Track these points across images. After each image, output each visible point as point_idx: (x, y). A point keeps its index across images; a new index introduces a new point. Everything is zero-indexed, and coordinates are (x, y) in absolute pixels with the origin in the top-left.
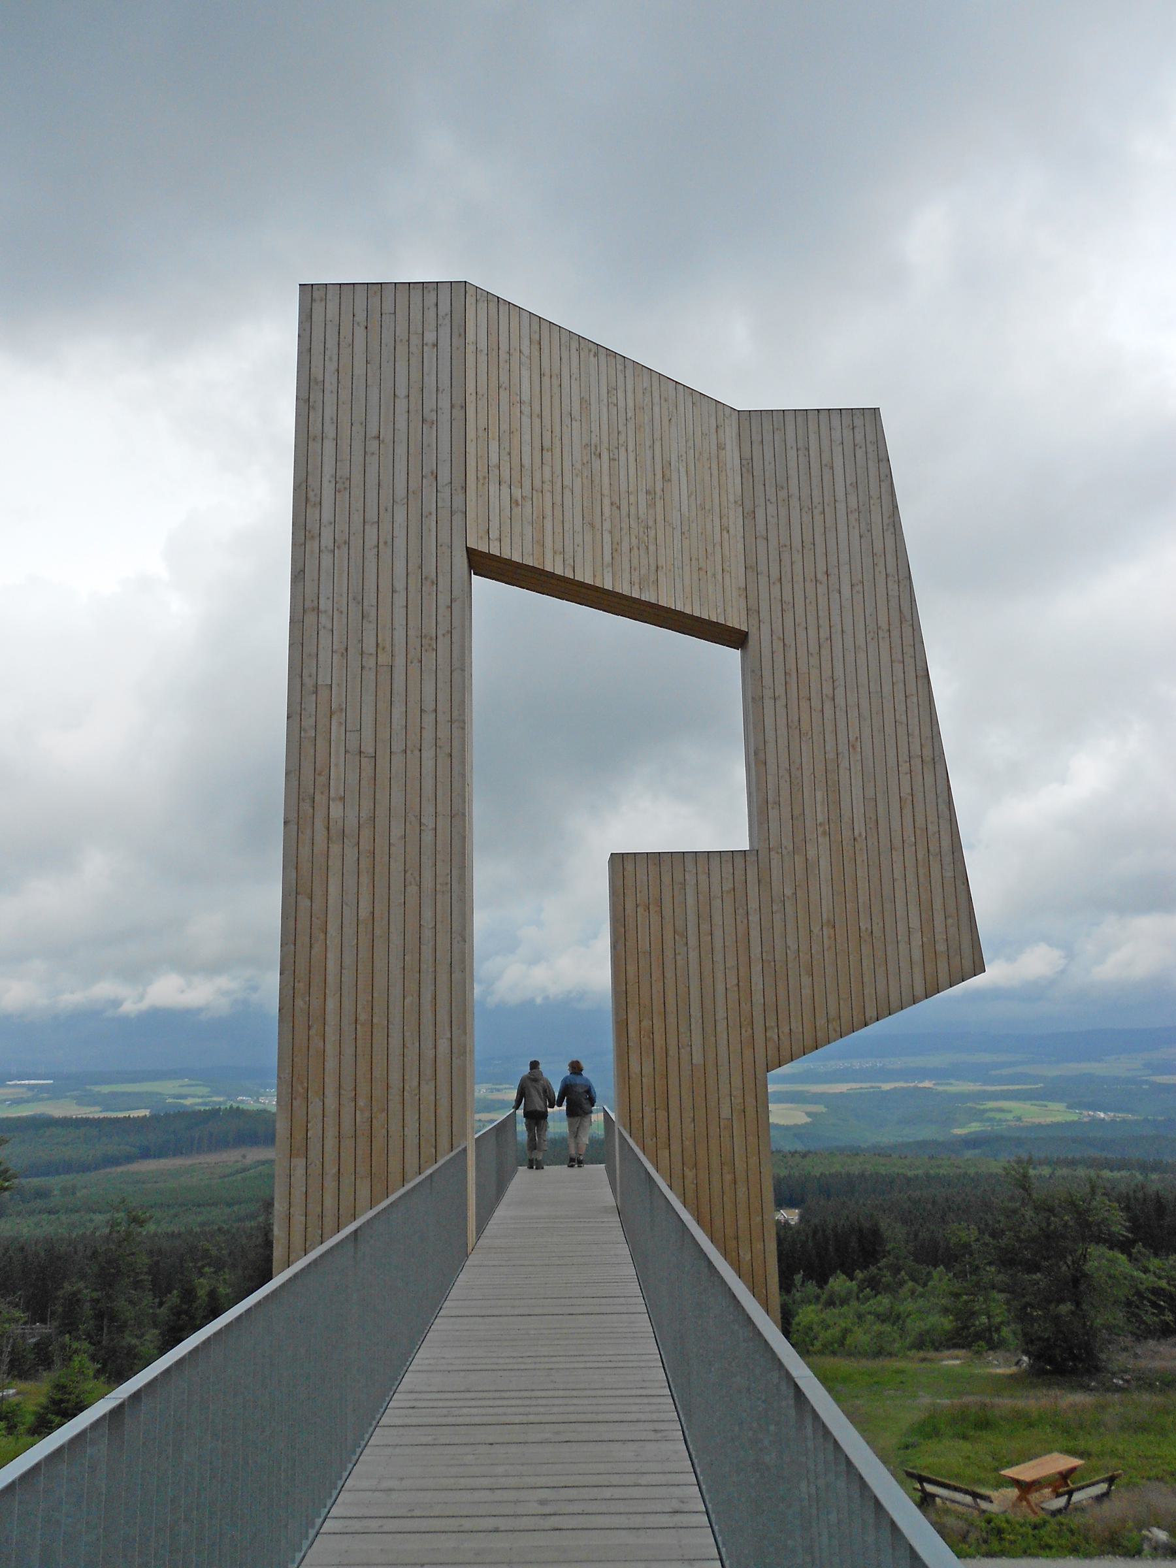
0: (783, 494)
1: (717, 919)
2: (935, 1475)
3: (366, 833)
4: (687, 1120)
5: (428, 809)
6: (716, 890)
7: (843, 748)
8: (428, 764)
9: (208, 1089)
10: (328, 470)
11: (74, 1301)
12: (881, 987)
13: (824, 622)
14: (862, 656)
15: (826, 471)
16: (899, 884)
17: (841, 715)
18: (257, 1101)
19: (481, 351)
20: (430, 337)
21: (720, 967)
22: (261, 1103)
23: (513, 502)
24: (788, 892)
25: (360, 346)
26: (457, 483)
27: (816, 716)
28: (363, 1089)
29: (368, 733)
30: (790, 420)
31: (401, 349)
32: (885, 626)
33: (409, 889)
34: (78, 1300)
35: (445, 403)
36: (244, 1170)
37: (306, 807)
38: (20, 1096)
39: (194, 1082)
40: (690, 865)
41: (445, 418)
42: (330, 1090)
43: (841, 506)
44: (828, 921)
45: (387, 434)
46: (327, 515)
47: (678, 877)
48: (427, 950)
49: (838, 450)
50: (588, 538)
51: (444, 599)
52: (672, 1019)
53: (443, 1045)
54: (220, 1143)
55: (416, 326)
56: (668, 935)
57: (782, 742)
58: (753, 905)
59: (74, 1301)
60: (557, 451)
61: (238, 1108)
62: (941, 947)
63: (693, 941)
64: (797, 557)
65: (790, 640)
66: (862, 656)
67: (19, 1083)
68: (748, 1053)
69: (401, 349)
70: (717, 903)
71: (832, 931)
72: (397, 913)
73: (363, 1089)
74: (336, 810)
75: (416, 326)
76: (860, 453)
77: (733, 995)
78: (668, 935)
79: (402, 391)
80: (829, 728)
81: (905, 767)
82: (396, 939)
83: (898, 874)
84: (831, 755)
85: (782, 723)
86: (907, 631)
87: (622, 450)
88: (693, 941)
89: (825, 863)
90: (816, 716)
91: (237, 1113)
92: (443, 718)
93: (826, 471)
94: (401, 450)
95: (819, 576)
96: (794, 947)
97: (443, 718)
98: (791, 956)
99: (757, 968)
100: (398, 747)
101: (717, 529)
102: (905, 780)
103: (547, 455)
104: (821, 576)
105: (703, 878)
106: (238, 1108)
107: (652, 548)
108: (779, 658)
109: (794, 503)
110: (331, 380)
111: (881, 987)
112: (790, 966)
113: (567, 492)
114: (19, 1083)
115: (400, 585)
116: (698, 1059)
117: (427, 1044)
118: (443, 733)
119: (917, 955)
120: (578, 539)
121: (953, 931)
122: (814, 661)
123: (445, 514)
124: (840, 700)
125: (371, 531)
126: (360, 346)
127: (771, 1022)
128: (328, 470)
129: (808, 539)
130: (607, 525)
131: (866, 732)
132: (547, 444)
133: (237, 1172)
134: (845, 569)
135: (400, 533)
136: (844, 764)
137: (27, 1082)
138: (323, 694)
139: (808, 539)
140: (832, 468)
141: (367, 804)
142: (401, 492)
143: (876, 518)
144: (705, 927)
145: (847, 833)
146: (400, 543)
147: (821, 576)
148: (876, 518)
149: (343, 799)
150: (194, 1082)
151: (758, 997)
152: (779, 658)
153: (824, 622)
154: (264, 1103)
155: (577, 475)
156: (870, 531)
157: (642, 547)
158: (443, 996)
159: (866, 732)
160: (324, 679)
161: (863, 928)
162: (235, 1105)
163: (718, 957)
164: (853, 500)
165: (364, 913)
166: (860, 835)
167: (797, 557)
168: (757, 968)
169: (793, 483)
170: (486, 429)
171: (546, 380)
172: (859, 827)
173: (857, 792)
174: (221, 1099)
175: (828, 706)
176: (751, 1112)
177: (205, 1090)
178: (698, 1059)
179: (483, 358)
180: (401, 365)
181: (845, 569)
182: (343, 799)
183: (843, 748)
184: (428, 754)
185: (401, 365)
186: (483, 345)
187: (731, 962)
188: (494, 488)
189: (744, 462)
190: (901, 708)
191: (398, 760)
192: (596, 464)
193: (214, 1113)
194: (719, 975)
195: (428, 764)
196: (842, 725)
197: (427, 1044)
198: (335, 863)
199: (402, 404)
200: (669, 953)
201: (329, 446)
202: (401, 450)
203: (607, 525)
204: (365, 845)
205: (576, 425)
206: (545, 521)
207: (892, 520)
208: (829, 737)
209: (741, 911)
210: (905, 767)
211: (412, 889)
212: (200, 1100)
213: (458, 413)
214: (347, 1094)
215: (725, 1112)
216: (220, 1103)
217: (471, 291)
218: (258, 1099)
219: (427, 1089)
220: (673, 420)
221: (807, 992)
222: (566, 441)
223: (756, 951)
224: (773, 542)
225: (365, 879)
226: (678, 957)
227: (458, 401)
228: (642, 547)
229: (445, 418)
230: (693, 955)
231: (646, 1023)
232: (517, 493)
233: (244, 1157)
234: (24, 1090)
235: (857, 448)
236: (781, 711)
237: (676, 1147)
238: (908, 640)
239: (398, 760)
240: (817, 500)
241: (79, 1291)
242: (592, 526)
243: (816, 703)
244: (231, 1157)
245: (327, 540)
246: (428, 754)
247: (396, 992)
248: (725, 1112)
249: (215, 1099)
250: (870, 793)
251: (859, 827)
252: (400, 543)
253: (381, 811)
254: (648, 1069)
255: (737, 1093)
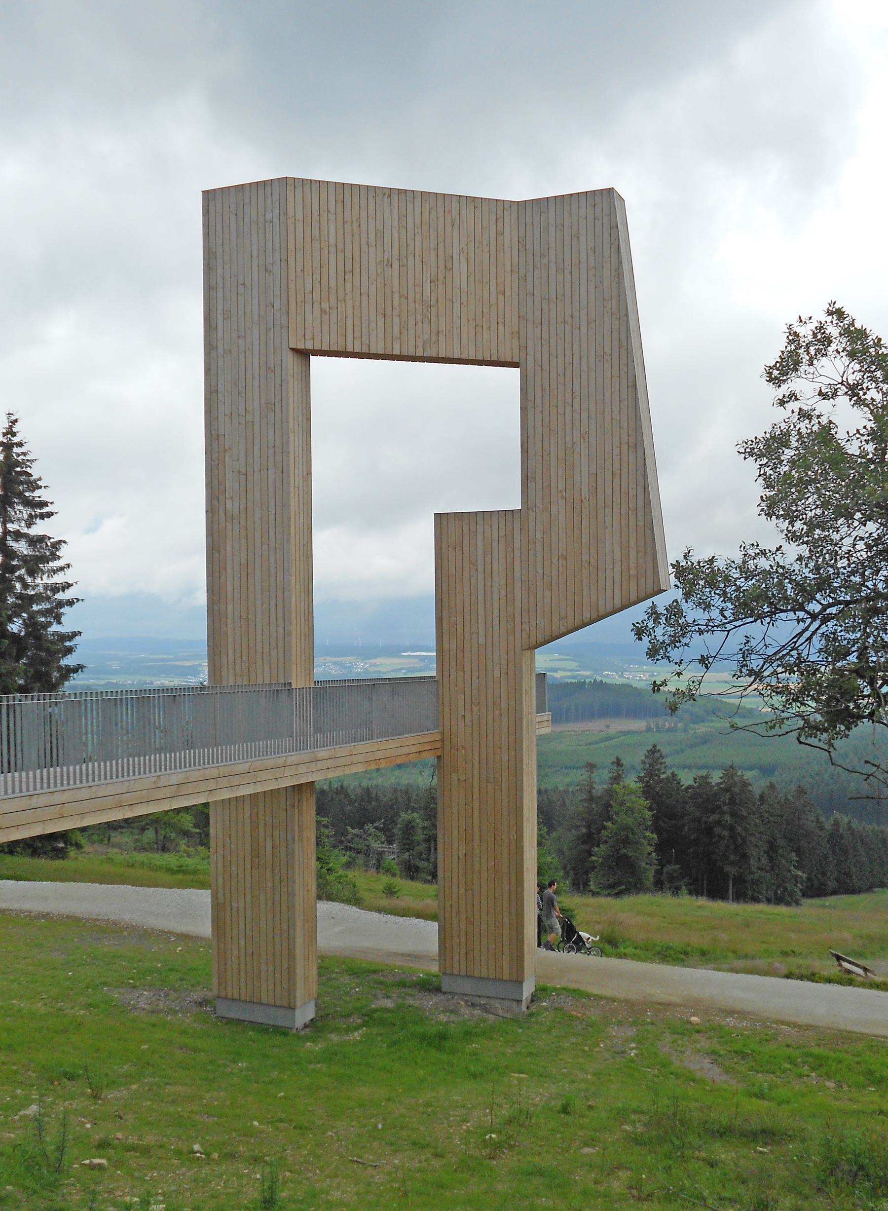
0: (545, 261)
1: (495, 554)
2: (844, 954)
3: (243, 516)
4: (474, 678)
5: (272, 503)
6: (495, 536)
7: (577, 438)
8: (271, 477)
9: (577, 664)
10: (220, 307)
11: (409, 828)
12: (594, 598)
13: (569, 353)
14: (593, 374)
15: (575, 240)
16: (609, 531)
17: (576, 416)
18: (622, 676)
19: (299, 220)
20: (269, 216)
21: (496, 585)
22: (625, 677)
23: (322, 312)
24: (539, 536)
25: (233, 226)
26: (284, 310)
27: (560, 418)
28: (245, 652)
29: (242, 459)
30: (551, 203)
31: (254, 226)
32: (609, 352)
33: (263, 547)
34: (413, 827)
35: (277, 260)
36: (609, 739)
37: (215, 502)
38: (412, 666)
39: (562, 657)
40: (480, 520)
41: (277, 268)
42: (230, 652)
43: (583, 266)
44: (562, 555)
45: (248, 283)
46: (220, 335)
47: (473, 528)
48: (272, 579)
49: (583, 222)
50: (381, 323)
51: (278, 381)
52: (467, 616)
53: (281, 630)
54: (589, 713)
55: (261, 211)
56: (466, 564)
57: (539, 436)
58: (517, 545)
59: (409, 828)
60: (356, 272)
61: (601, 681)
62: (633, 572)
63: (480, 569)
64: (553, 306)
65: (546, 367)
66: (593, 374)
67: (412, 654)
68: (511, 638)
69: (254, 226)
70: (495, 544)
71: (565, 562)
72: (258, 560)
73: (245, 652)
74: (229, 504)
75: (261, 211)
76: (598, 223)
77: (503, 603)
78: (466, 564)
79: (255, 254)
80: (568, 426)
81: (616, 451)
82: (258, 574)
83: (608, 524)
84: (569, 445)
85: (539, 423)
86: (624, 353)
87: (411, 258)
88: (480, 569)
89: (562, 518)
90: (560, 418)
91: (600, 686)
92: (278, 450)
93: (575, 240)
94: (255, 290)
95: (566, 319)
96: (540, 571)
97: (278, 450)
98: (539, 579)
99: (518, 586)
100: (257, 468)
101: (494, 293)
102: (616, 459)
103: (349, 276)
104: (568, 319)
105: (488, 530)
106: (601, 681)
107: (434, 319)
108: (538, 378)
109: (553, 267)
110: (219, 250)
111: (594, 598)
112: (538, 583)
113: (365, 298)
114: (412, 654)
115: (256, 374)
116: (482, 641)
117: (273, 629)
118: (278, 459)
119: (617, 577)
120: (373, 325)
121: (641, 561)
122: (561, 379)
123: (278, 328)
124: (577, 407)
125: (241, 341)
126: (233, 226)
127: (525, 619)
128: (220, 307)
129: (560, 292)
130: (396, 312)
131: (593, 427)
132: (349, 267)
133: (602, 741)
134: (584, 313)
135: (256, 343)
136: (577, 450)
137: (418, 653)
138: (221, 439)
139: (560, 292)
140: (578, 238)
141: (243, 501)
142: (256, 317)
143: (607, 273)
144: (488, 559)
145: (577, 496)
146: (256, 347)
147: (568, 319)
148: (607, 273)
149: (232, 498)
150: (562, 657)
151: (518, 603)
152: (538, 378)
153: (569, 353)
154: (628, 678)
155: (372, 284)
156: (602, 282)
157: (426, 320)
158: (280, 605)
159: (593, 427)
160: (221, 432)
161: (584, 560)
162: (599, 679)
163: (495, 579)
164: (591, 259)
165: (243, 561)
166: (585, 498)
167: (553, 306)
168: (518, 586)
169: (552, 252)
170: (303, 271)
171: (348, 226)
172: (585, 491)
173: (585, 468)
174: (588, 673)
175: (569, 409)
176: (511, 673)
177: (573, 665)
178: (482, 641)
179: (299, 225)
180: (255, 236)
181: (584, 313)
182: (232, 498)
183: (577, 438)
184: (271, 472)
185: (255, 236)
186: (299, 216)
187: (503, 582)
188: (308, 307)
189: (521, 240)
190: (616, 409)
191: (257, 476)
192: (388, 271)
193: (580, 686)
194: (495, 589)
195: (271, 477)
196: (577, 424)
197: (273, 629)
198: (229, 533)
199: (255, 260)
200: (466, 576)
201: (220, 292)
202: (255, 290)
203: (396, 312)
204: (243, 523)
205: (372, 250)
206: (347, 320)
207: (617, 272)
208: (568, 431)
209: (509, 549)
210: (616, 451)
211: (265, 547)
212: (569, 674)
213: (284, 264)
214: (238, 654)
215: (497, 674)
216: (588, 677)
217: (290, 182)
218: (622, 674)
219: (274, 652)
220: (456, 225)
221: (547, 600)
222: (364, 262)
223: (517, 574)
224: (538, 298)
225: (243, 542)
226: (472, 578)
227: (284, 258)
228: (426, 320)
229: (277, 268)
230: (481, 576)
231: (453, 619)
232: (325, 306)
233: (608, 726)
234: (416, 660)
235: (596, 220)
236: (539, 416)
237: (468, 692)
238: (624, 361)
239: (257, 476)
240: (567, 262)
241: (414, 820)
242: (385, 315)
243: (561, 410)
244: (596, 726)
245: (221, 351)
246: (271, 472)
247: (259, 603)
248: (497, 674)
249: (581, 673)
250: (593, 470)
251: (585, 491)
252: (256, 347)
253: (250, 504)
254: (453, 646)
255: (504, 662)
